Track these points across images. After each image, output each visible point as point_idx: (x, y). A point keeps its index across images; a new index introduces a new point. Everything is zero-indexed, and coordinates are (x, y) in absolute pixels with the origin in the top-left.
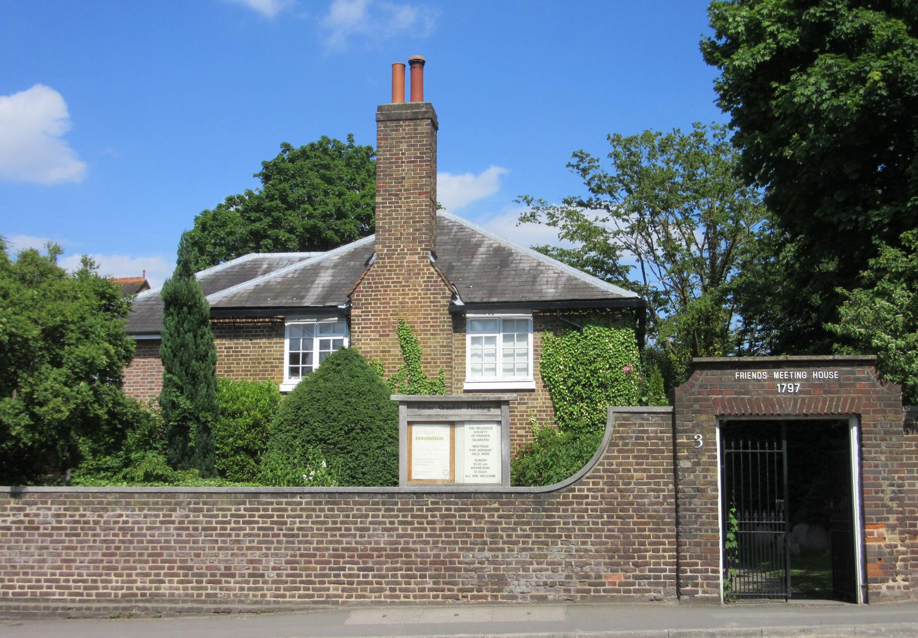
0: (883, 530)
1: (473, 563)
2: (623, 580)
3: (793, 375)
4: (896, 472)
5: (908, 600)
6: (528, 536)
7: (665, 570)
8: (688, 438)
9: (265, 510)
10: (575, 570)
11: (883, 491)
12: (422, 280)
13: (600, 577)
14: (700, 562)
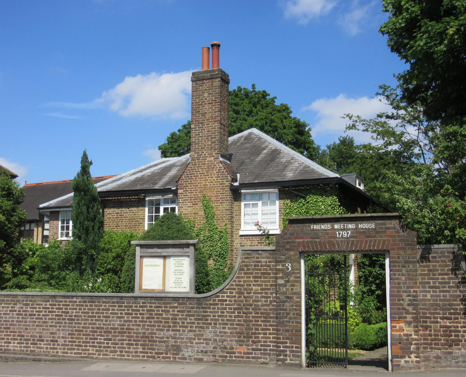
0: (402, 325)
1: (163, 338)
2: (246, 351)
3: (347, 226)
4: (412, 287)
5: (418, 370)
6: (193, 323)
7: (270, 346)
8: (283, 266)
9: (59, 305)
10: (219, 344)
11: (403, 300)
13: (232, 348)
14: (288, 341)
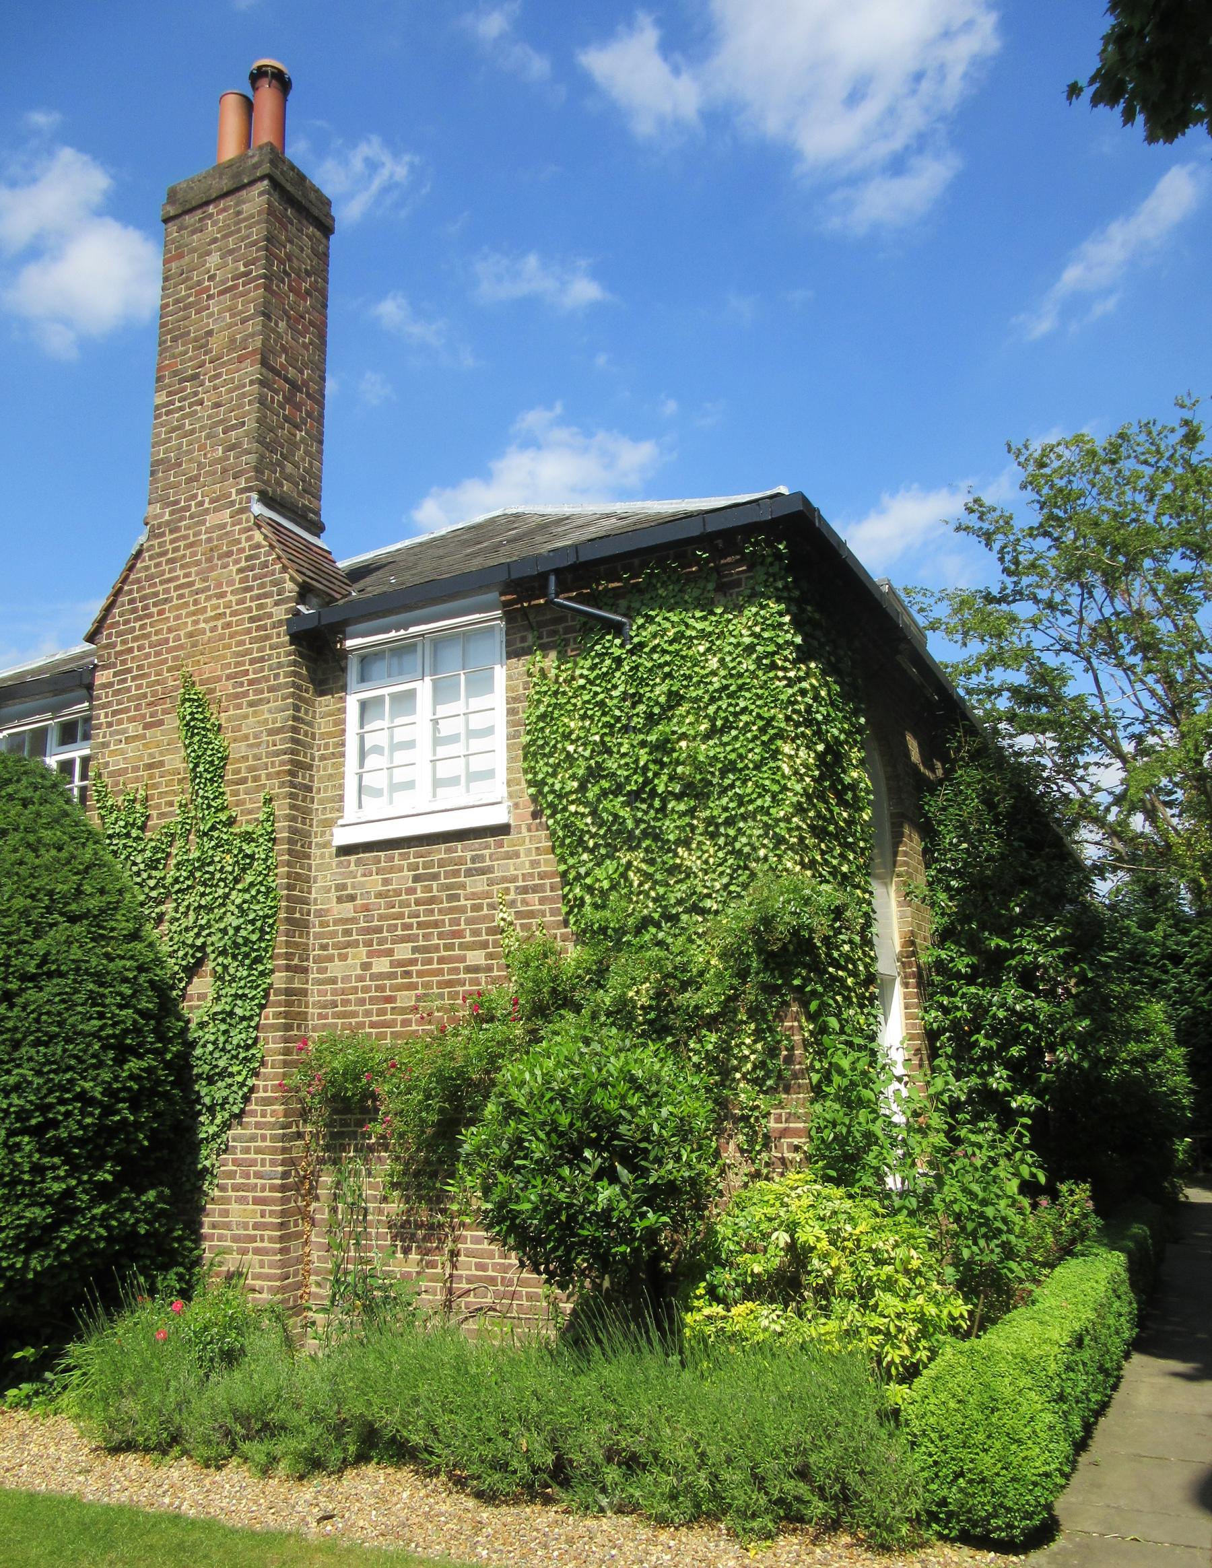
12: (234, 569)
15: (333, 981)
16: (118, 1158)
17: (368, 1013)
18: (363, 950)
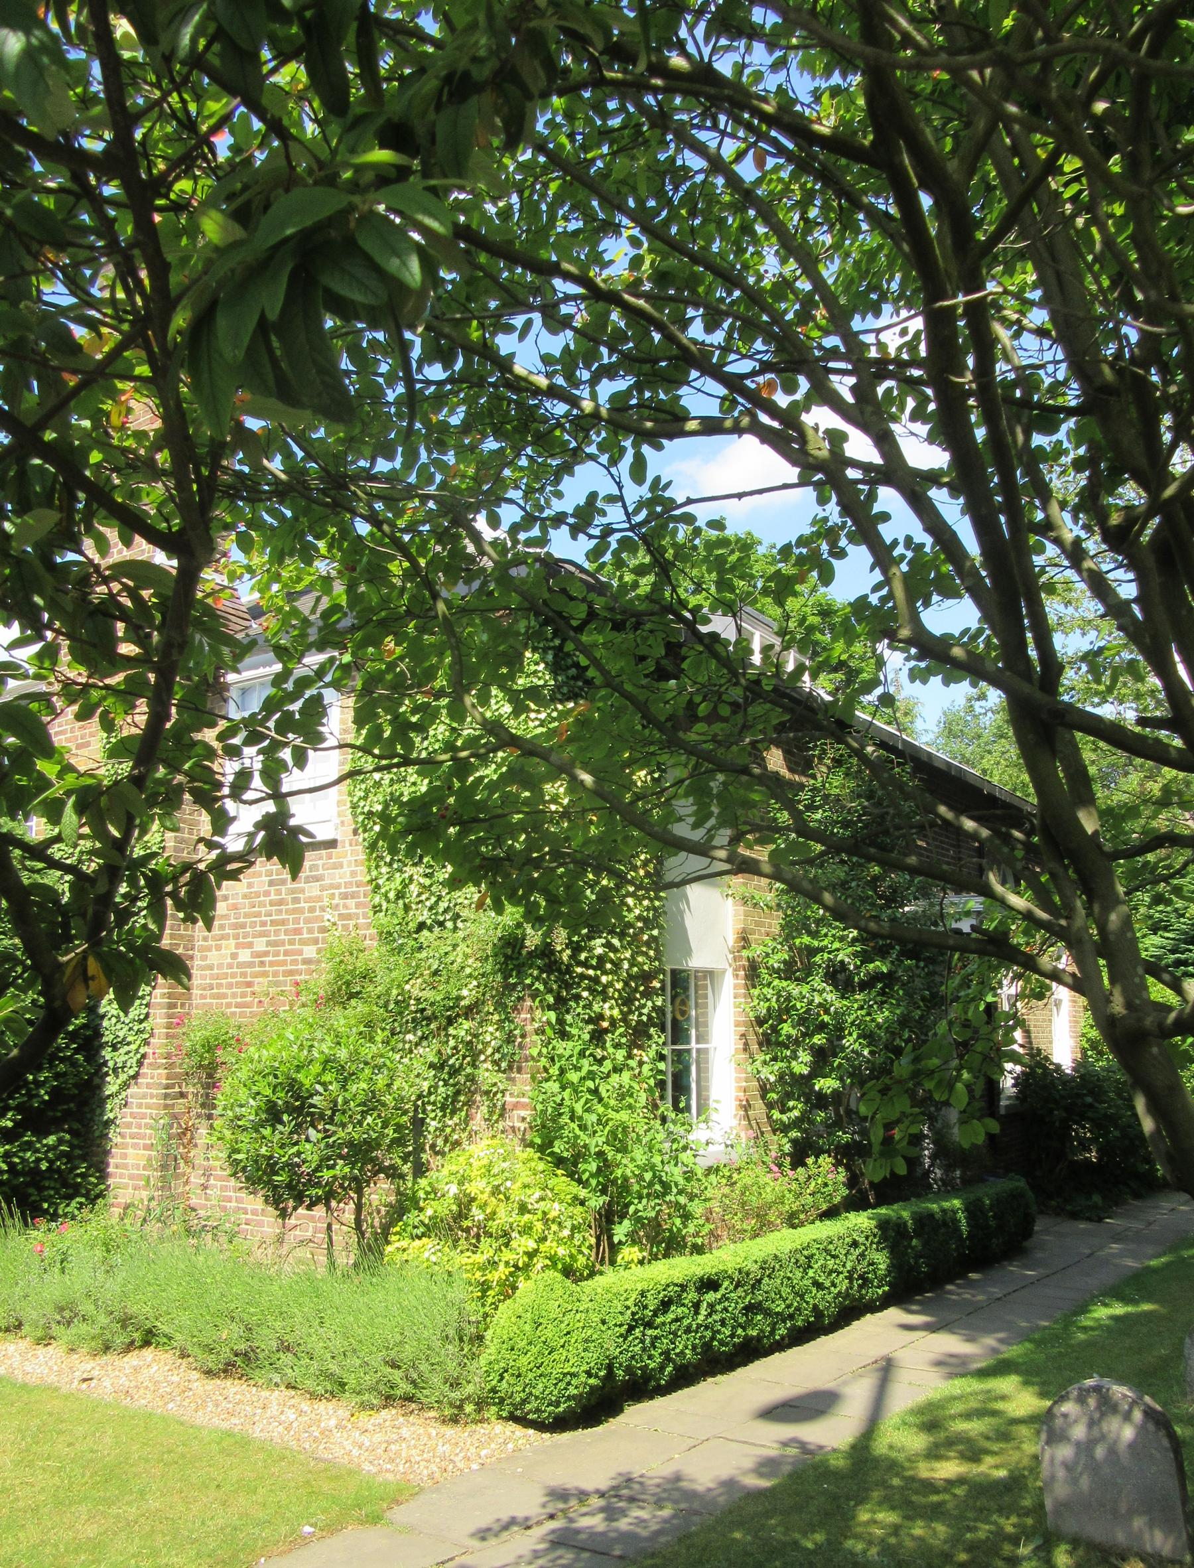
15: (211, 968)
16: (19, 1109)
17: (234, 995)
18: (232, 942)
